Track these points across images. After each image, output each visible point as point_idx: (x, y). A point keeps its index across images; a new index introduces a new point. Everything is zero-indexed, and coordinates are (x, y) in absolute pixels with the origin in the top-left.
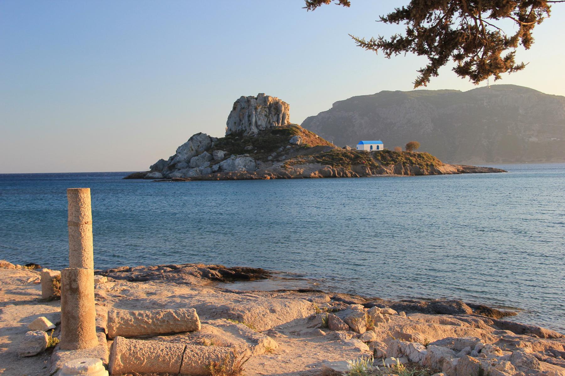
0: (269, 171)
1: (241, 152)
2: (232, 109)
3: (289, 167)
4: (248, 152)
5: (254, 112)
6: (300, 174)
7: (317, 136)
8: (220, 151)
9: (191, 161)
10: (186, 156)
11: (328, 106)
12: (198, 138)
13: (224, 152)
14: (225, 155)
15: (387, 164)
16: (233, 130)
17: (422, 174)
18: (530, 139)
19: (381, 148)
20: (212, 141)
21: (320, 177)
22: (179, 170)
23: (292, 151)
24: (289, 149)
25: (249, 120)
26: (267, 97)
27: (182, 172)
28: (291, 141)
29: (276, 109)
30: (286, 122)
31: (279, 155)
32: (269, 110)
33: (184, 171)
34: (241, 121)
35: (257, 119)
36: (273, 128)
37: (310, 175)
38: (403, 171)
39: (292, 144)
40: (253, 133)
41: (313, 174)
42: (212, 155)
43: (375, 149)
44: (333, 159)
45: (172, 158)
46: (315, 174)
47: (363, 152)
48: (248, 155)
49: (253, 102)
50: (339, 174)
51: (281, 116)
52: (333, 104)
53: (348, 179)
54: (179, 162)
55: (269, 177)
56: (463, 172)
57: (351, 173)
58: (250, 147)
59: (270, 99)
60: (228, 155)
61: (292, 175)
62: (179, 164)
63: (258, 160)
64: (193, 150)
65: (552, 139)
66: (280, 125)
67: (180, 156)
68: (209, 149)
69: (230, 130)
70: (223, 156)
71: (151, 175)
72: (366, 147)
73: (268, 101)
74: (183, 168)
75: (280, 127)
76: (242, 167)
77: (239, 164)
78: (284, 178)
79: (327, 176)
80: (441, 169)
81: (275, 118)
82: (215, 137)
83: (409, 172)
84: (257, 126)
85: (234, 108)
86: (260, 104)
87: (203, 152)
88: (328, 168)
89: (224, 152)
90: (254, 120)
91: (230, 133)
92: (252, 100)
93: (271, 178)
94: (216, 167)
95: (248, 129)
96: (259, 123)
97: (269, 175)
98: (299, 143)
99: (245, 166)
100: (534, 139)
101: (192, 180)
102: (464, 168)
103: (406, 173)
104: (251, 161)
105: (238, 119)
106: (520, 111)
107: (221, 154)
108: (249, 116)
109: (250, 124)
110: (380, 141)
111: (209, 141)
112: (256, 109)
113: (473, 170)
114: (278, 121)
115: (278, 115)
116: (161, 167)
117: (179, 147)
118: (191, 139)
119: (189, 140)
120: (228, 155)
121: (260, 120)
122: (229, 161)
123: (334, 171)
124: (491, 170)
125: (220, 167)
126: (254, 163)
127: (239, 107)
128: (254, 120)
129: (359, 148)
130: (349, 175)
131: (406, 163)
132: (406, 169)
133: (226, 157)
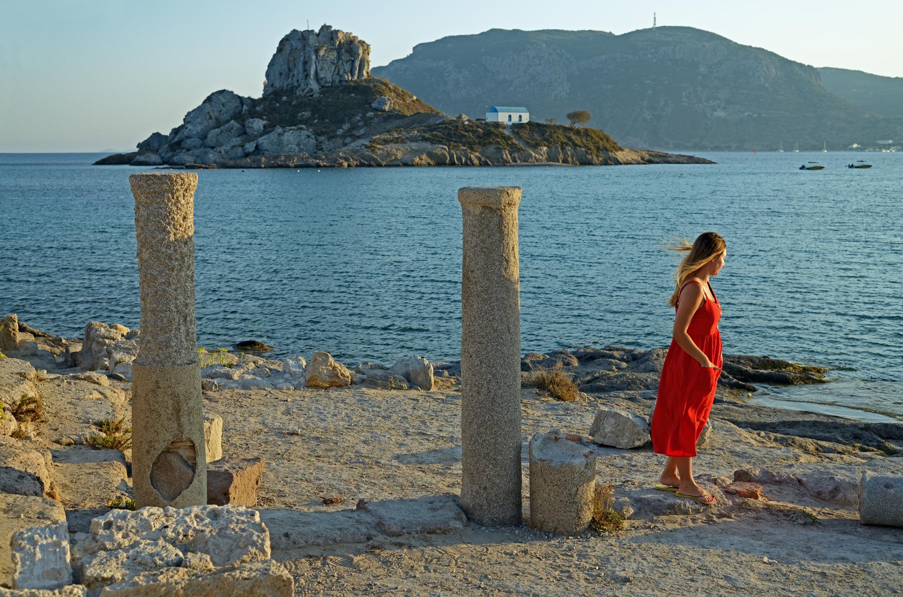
0: (345, 153)
1: (292, 121)
2: (275, 52)
3: (379, 146)
4: (306, 122)
5: (314, 57)
6: (396, 159)
7: (415, 98)
8: (257, 120)
9: (209, 136)
10: (199, 128)
11: (406, 52)
12: (221, 97)
13: (265, 122)
14: (264, 126)
15: (535, 146)
16: (278, 85)
17: (590, 163)
18: (715, 114)
19: (526, 118)
20: (242, 104)
21: (429, 165)
22: (188, 150)
23: (376, 120)
24: (371, 118)
25: (305, 70)
26: (337, 32)
27: (193, 155)
28: (374, 105)
29: (350, 49)
30: (365, 74)
31: (354, 127)
32: (338, 53)
33: (197, 152)
34: (290, 70)
35: (319, 68)
36: (344, 84)
37: (413, 161)
38: (561, 157)
39: (376, 110)
40: (312, 90)
41: (417, 160)
42: (243, 126)
43: (515, 119)
44: (449, 135)
45: (175, 131)
46: (421, 159)
47: (497, 125)
48: (304, 126)
49: (312, 40)
50: (459, 159)
51: (357, 64)
52: (414, 48)
53: (473, 169)
54: (188, 137)
55: (345, 164)
56: (650, 162)
57: (479, 159)
58: (307, 114)
59: (340, 36)
60: (270, 126)
61: (383, 160)
62: (188, 141)
63: (320, 135)
64: (211, 118)
65: (746, 114)
66: (356, 78)
67: (190, 127)
68: (238, 116)
69: (272, 85)
70: (262, 128)
71: (142, 158)
72: (502, 117)
73: (337, 38)
74: (195, 147)
75: (355, 81)
76: (294, 146)
77: (289, 142)
78: (370, 166)
79: (440, 163)
80: (620, 155)
81: (347, 67)
82: (246, 96)
83: (570, 159)
84: (317, 79)
85: (280, 50)
86: (324, 43)
87: (228, 121)
88: (440, 149)
89: (265, 122)
90: (312, 72)
91: (271, 90)
92: (311, 37)
93: (349, 166)
94: (250, 147)
95: (302, 85)
96: (322, 75)
97: (347, 159)
98: (387, 108)
99: (298, 145)
100: (720, 113)
101: (220, 168)
102: (650, 155)
103: (565, 161)
104: (308, 136)
105: (285, 67)
106: (702, 70)
107: (258, 124)
108: (305, 63)
109: (307, 76)
110: (524, 109)
111: (238, 104)
112: (317, 51)
113: (665, 159)
114: (352, 72)
115: (353, 62)
116: (156, 145)
117: (189, 113)
118: (209, 100)
119: (205, 102)
120: (270, 126)
121: (323, 67)
122: (273, 136)
123: (452, 157)
124: (692, 160)
125: (257, 147)
126: (314, 141)
127: (287, 48)
128: (312, 72)
129: (490, 118)
130: (476, 161)
131: (567, 144)
132: (565, 154)
133: (266, 130)
